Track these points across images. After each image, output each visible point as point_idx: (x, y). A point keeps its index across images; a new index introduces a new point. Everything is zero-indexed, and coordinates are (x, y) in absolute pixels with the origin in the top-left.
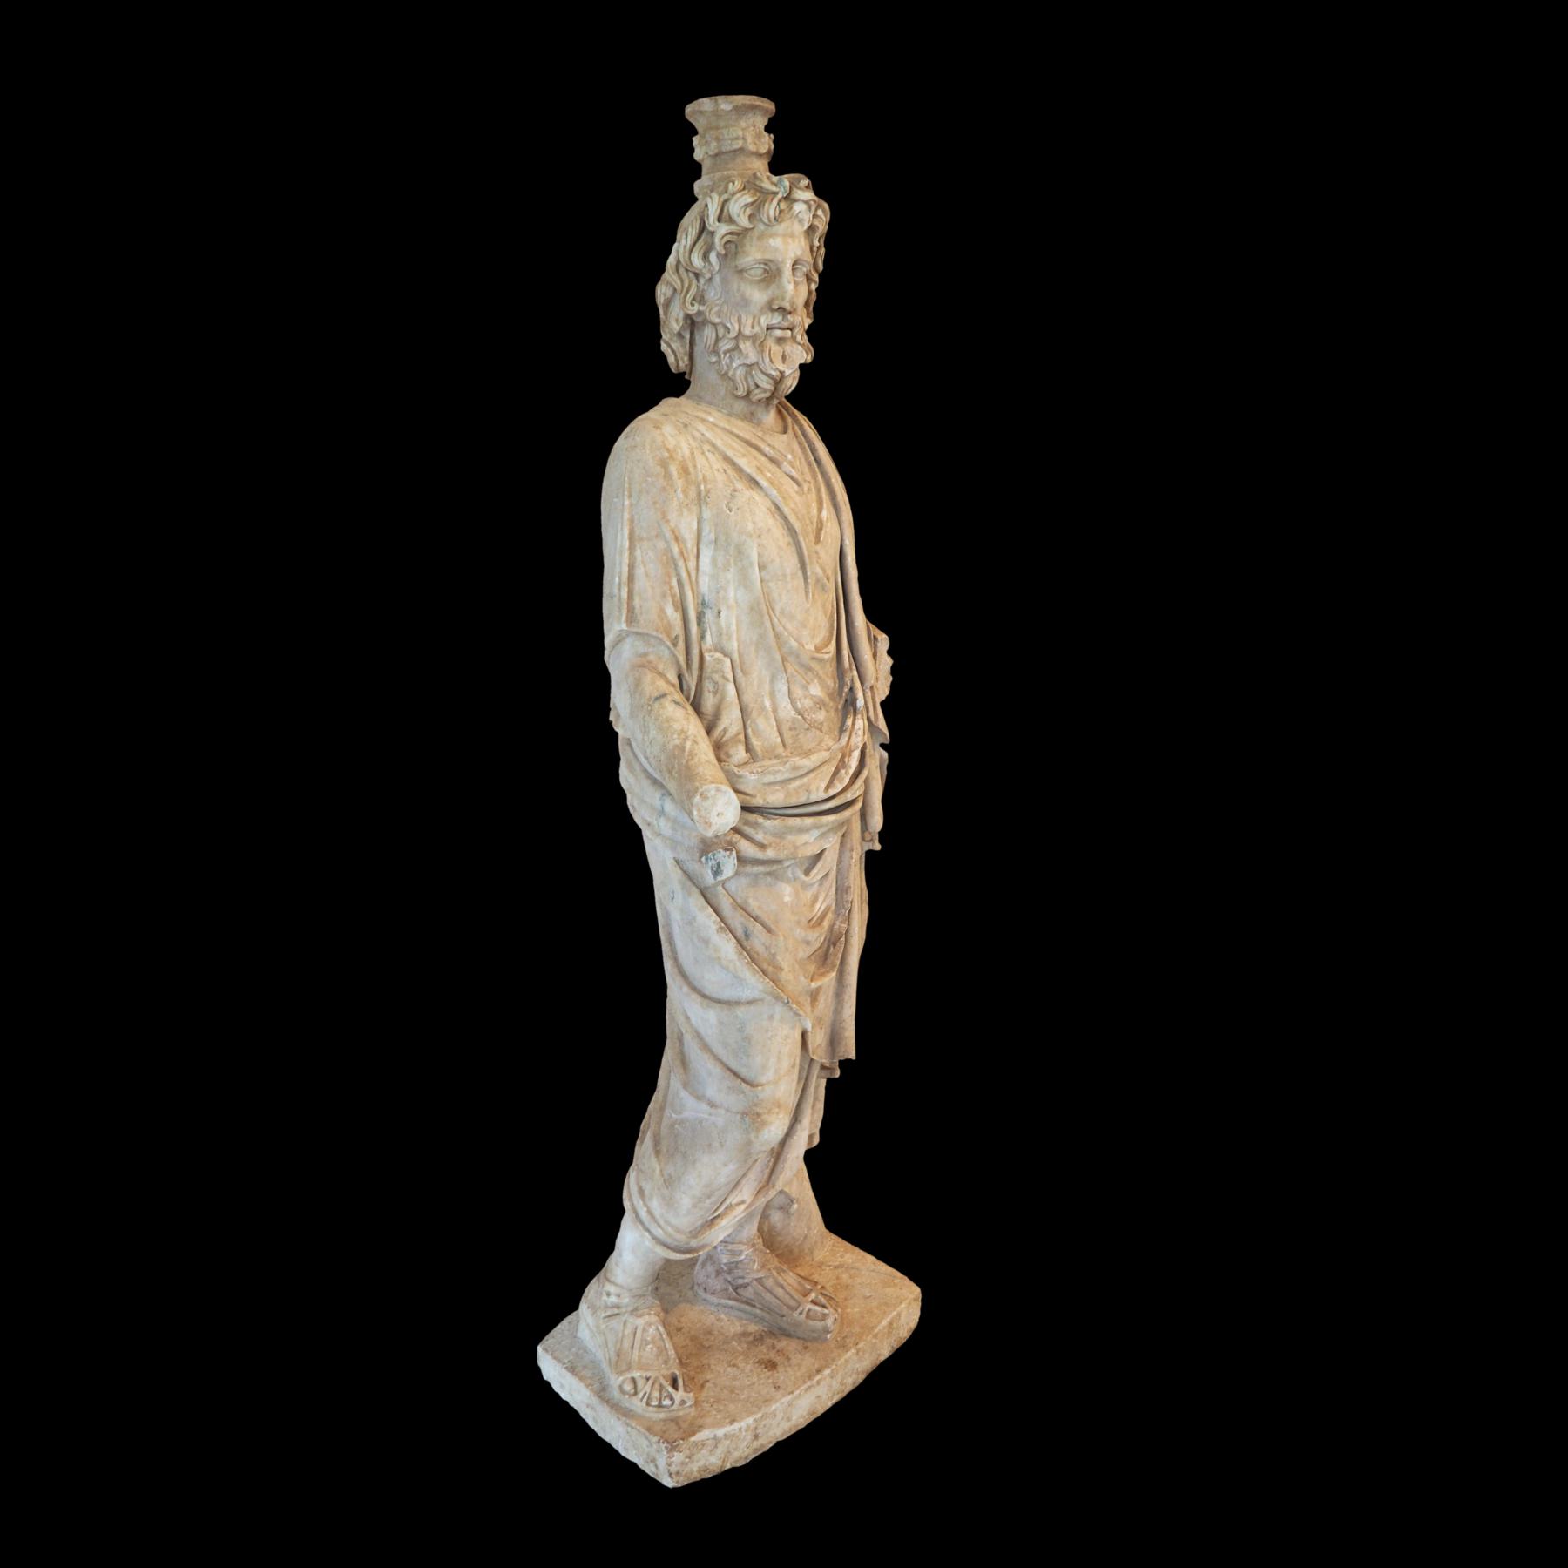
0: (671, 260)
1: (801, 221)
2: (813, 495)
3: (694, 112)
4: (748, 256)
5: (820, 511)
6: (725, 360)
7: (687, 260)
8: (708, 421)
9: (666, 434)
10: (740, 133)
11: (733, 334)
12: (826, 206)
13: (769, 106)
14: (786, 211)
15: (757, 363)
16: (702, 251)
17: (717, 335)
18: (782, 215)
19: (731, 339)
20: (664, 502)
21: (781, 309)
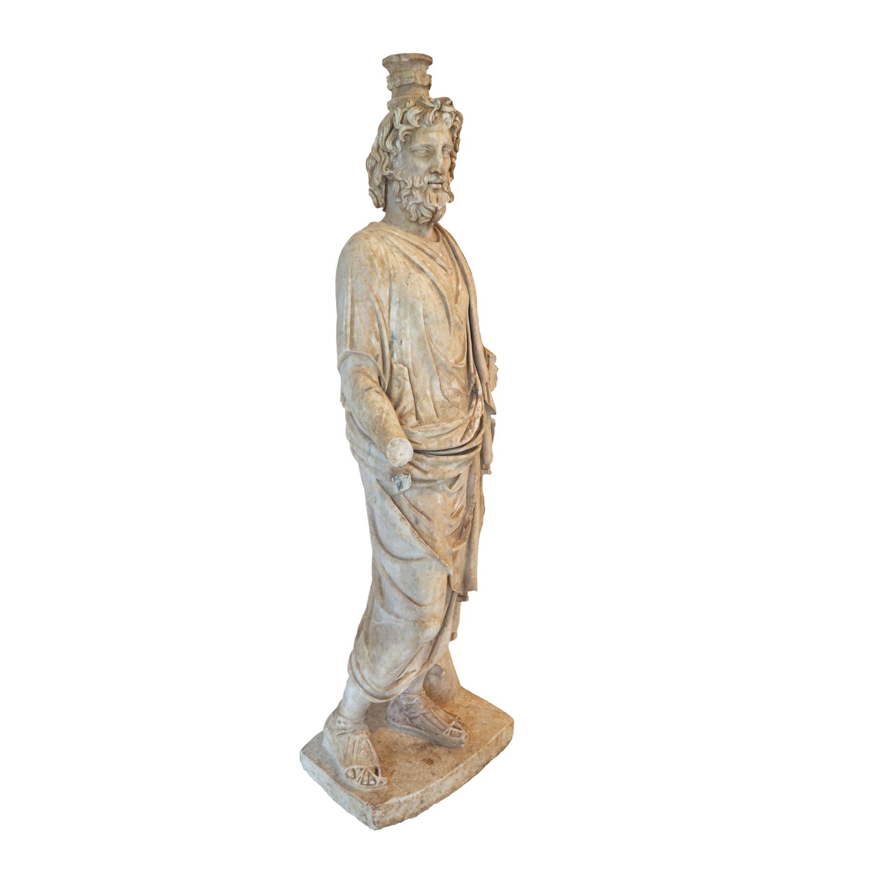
1: (447, 123)
2: (454, 276)
4: (417, 143)
5: (458, 285)
6: (405, 201)
7: (384, 145)
8: (395, 235)
9: (372, 242)
10: (413, 74)
11: (409, 186)
14: (439, 118)
15: (423, 203)
16: (392, 140)
17: (400, 187)
18: (436, 120)
19: (408, 189)
20: (371, 280)
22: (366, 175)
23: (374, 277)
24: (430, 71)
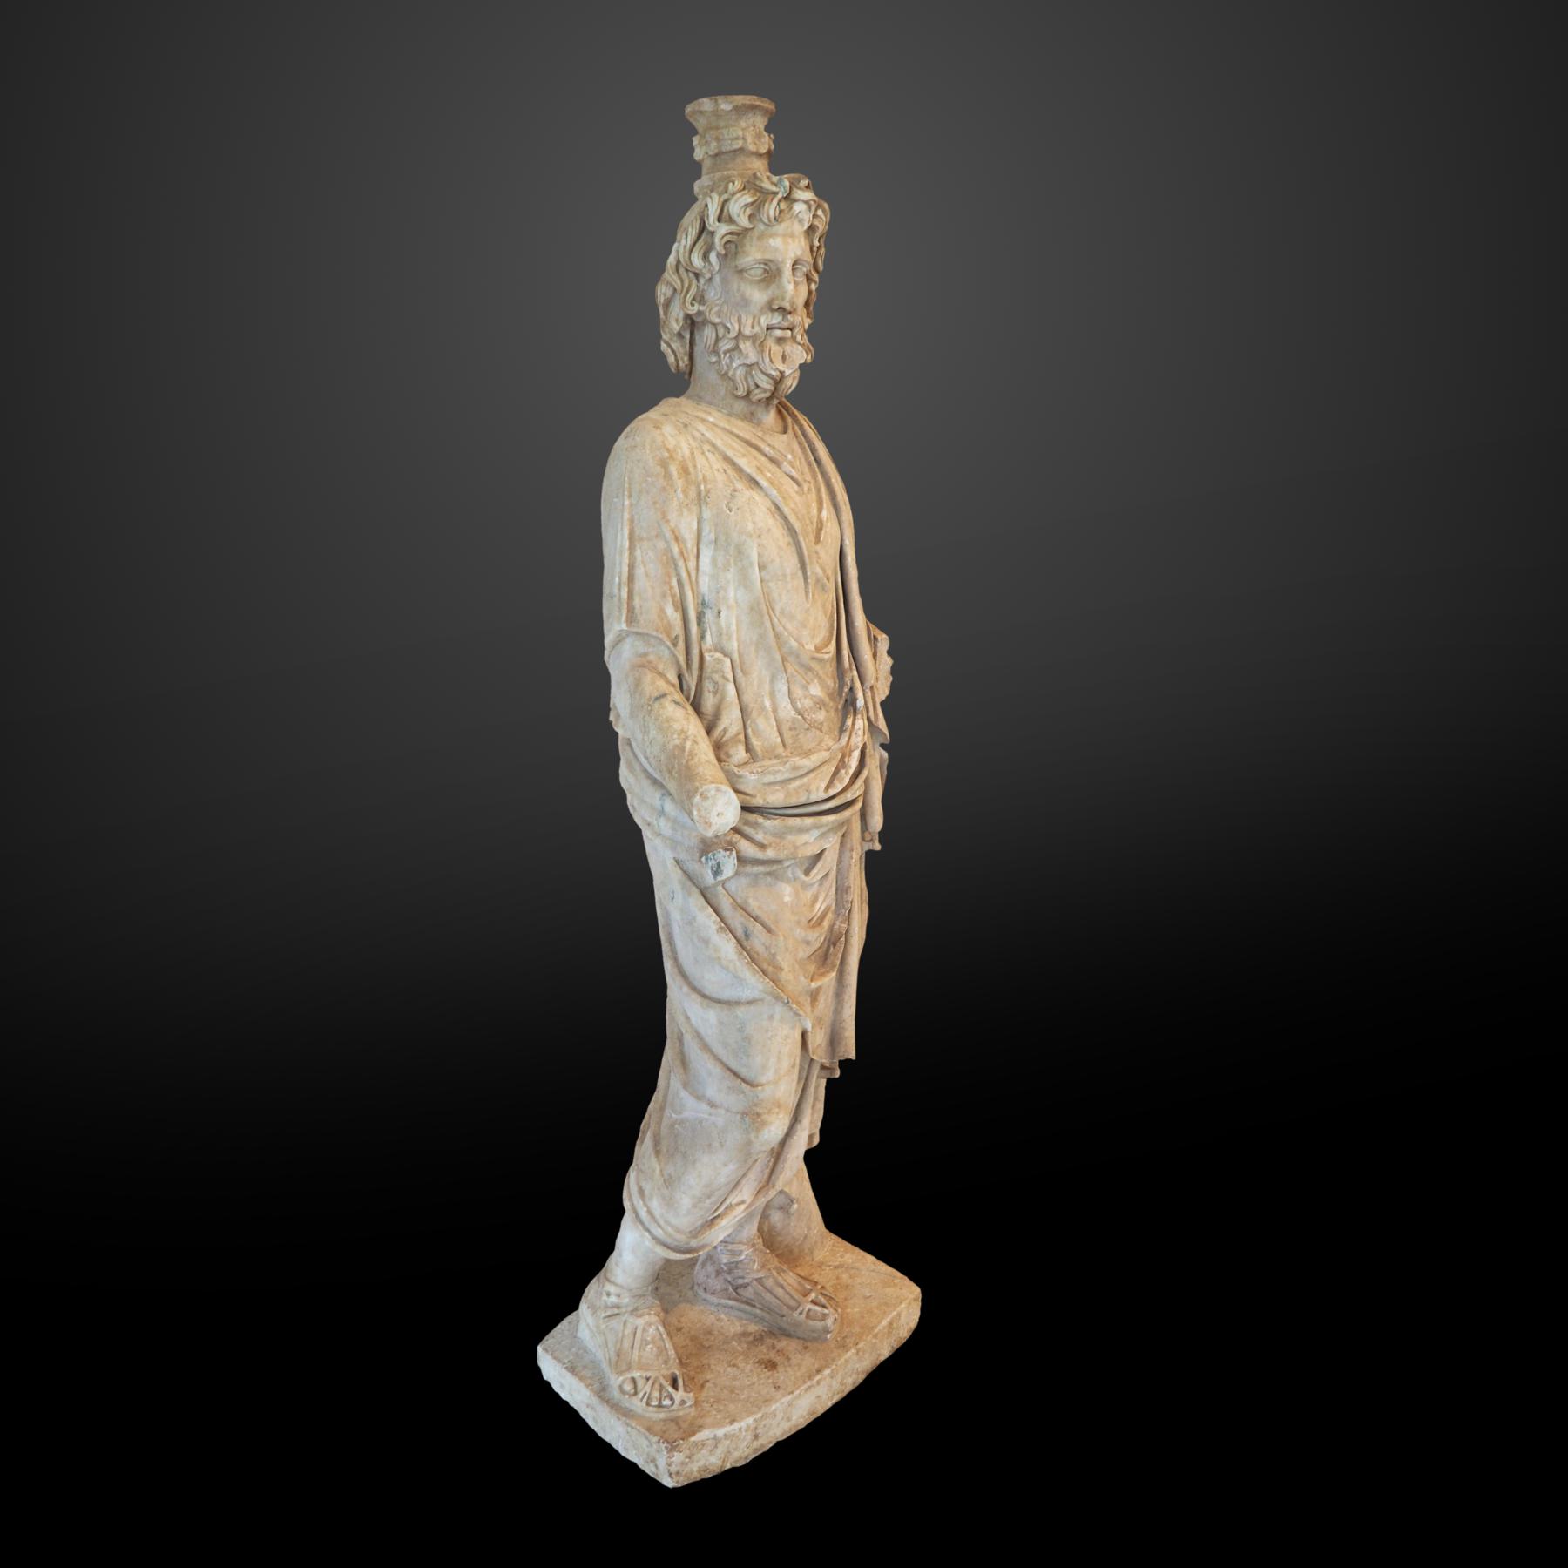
0: (671, 260)
1: (801, 221)
2: (813, 495)
3: (694, 112)
4: (748, 256)
5: (820, 511)
6: (725, 360)
7: (687, 260)
8: (708, 421)
9: (666, 434)
10: (740, 133)
11: (733, 334)
12: (826, 206)
13: (768, 105)
14: (786, 211)
15: (757, 363)
16: (702, 251)
17: (717, 335)
18: (782, 215)
19: (731, 339)
20: (664, 502)
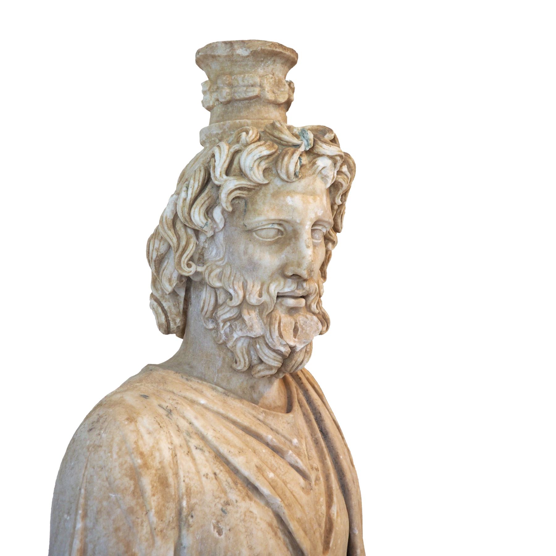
1: (324, 178)
2: (321, 487)
4: (259, 215)
5: (329, 505)
6: (224, 329)
7: (186, 215)
8: (199, 404)
9: (143, 430)
10: (258, 80)
11: (236, 302)
14: (308, 167)
15: (263, 337)
16: (204, 207)
17: (216, 300)
18: (303, 170)
19: (233, 307)
20: (130, 528)
21: (298, 278)
22: (147, 272)
23: (140, 520)
24: (292, 75)
